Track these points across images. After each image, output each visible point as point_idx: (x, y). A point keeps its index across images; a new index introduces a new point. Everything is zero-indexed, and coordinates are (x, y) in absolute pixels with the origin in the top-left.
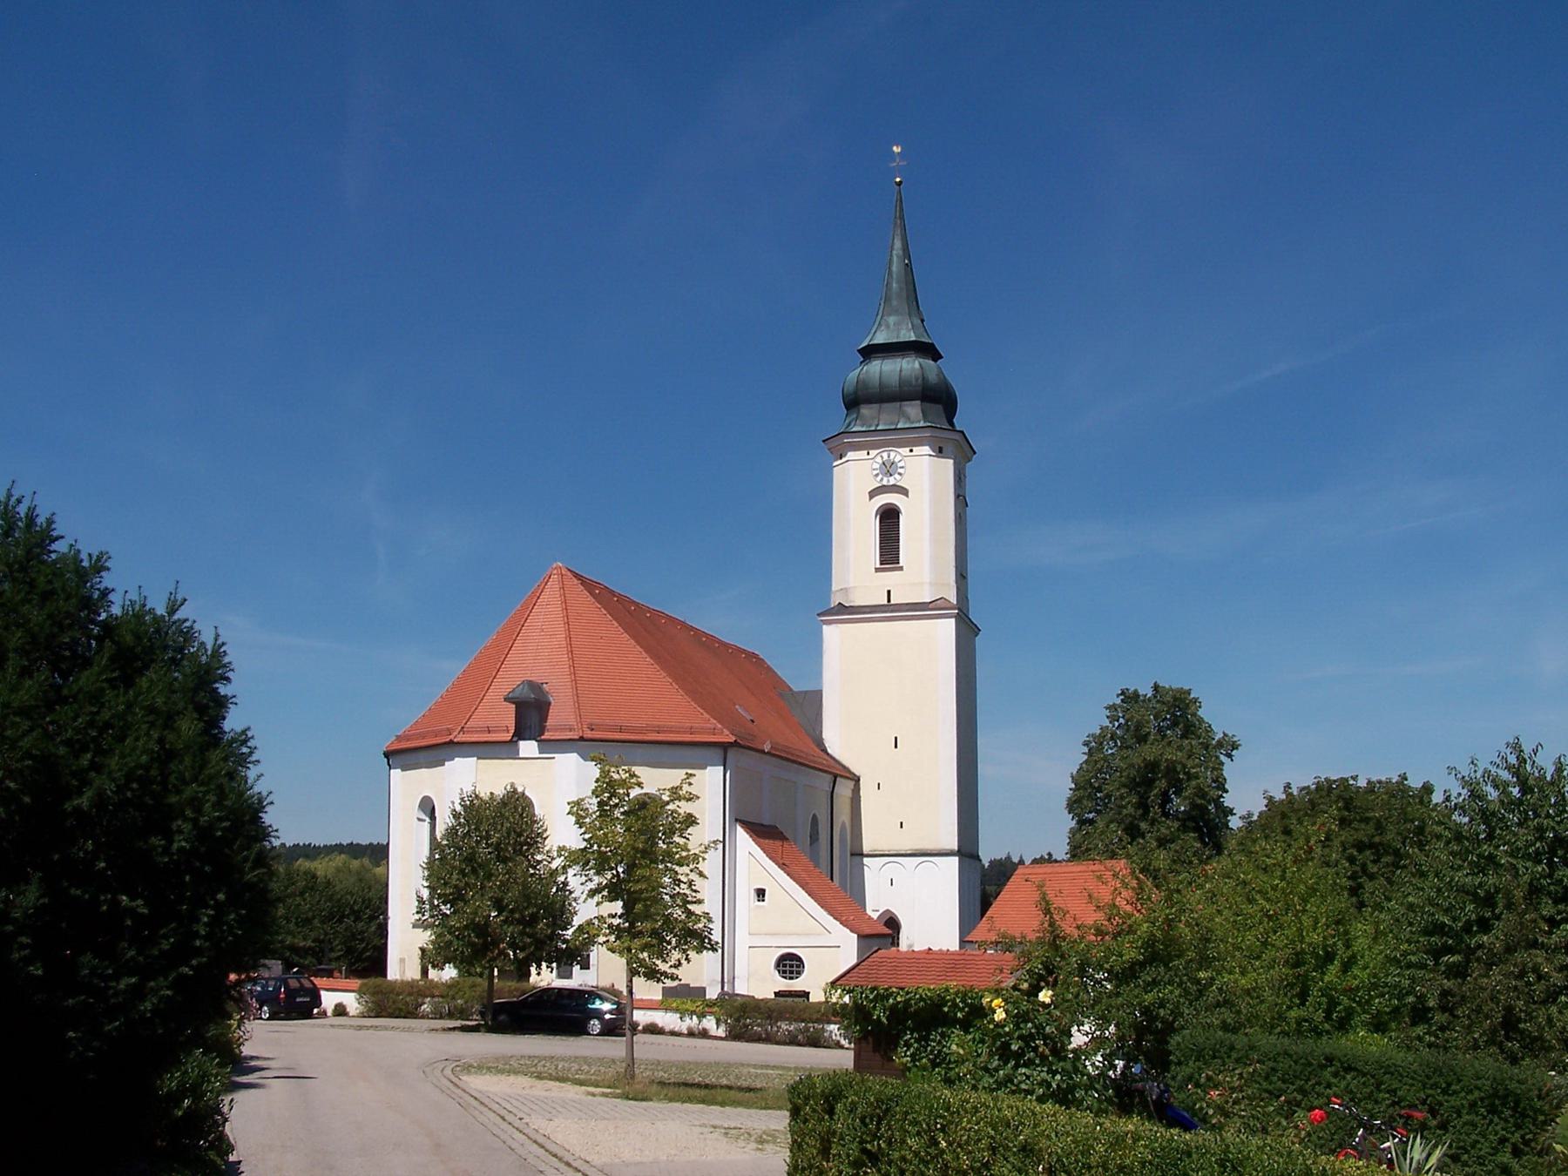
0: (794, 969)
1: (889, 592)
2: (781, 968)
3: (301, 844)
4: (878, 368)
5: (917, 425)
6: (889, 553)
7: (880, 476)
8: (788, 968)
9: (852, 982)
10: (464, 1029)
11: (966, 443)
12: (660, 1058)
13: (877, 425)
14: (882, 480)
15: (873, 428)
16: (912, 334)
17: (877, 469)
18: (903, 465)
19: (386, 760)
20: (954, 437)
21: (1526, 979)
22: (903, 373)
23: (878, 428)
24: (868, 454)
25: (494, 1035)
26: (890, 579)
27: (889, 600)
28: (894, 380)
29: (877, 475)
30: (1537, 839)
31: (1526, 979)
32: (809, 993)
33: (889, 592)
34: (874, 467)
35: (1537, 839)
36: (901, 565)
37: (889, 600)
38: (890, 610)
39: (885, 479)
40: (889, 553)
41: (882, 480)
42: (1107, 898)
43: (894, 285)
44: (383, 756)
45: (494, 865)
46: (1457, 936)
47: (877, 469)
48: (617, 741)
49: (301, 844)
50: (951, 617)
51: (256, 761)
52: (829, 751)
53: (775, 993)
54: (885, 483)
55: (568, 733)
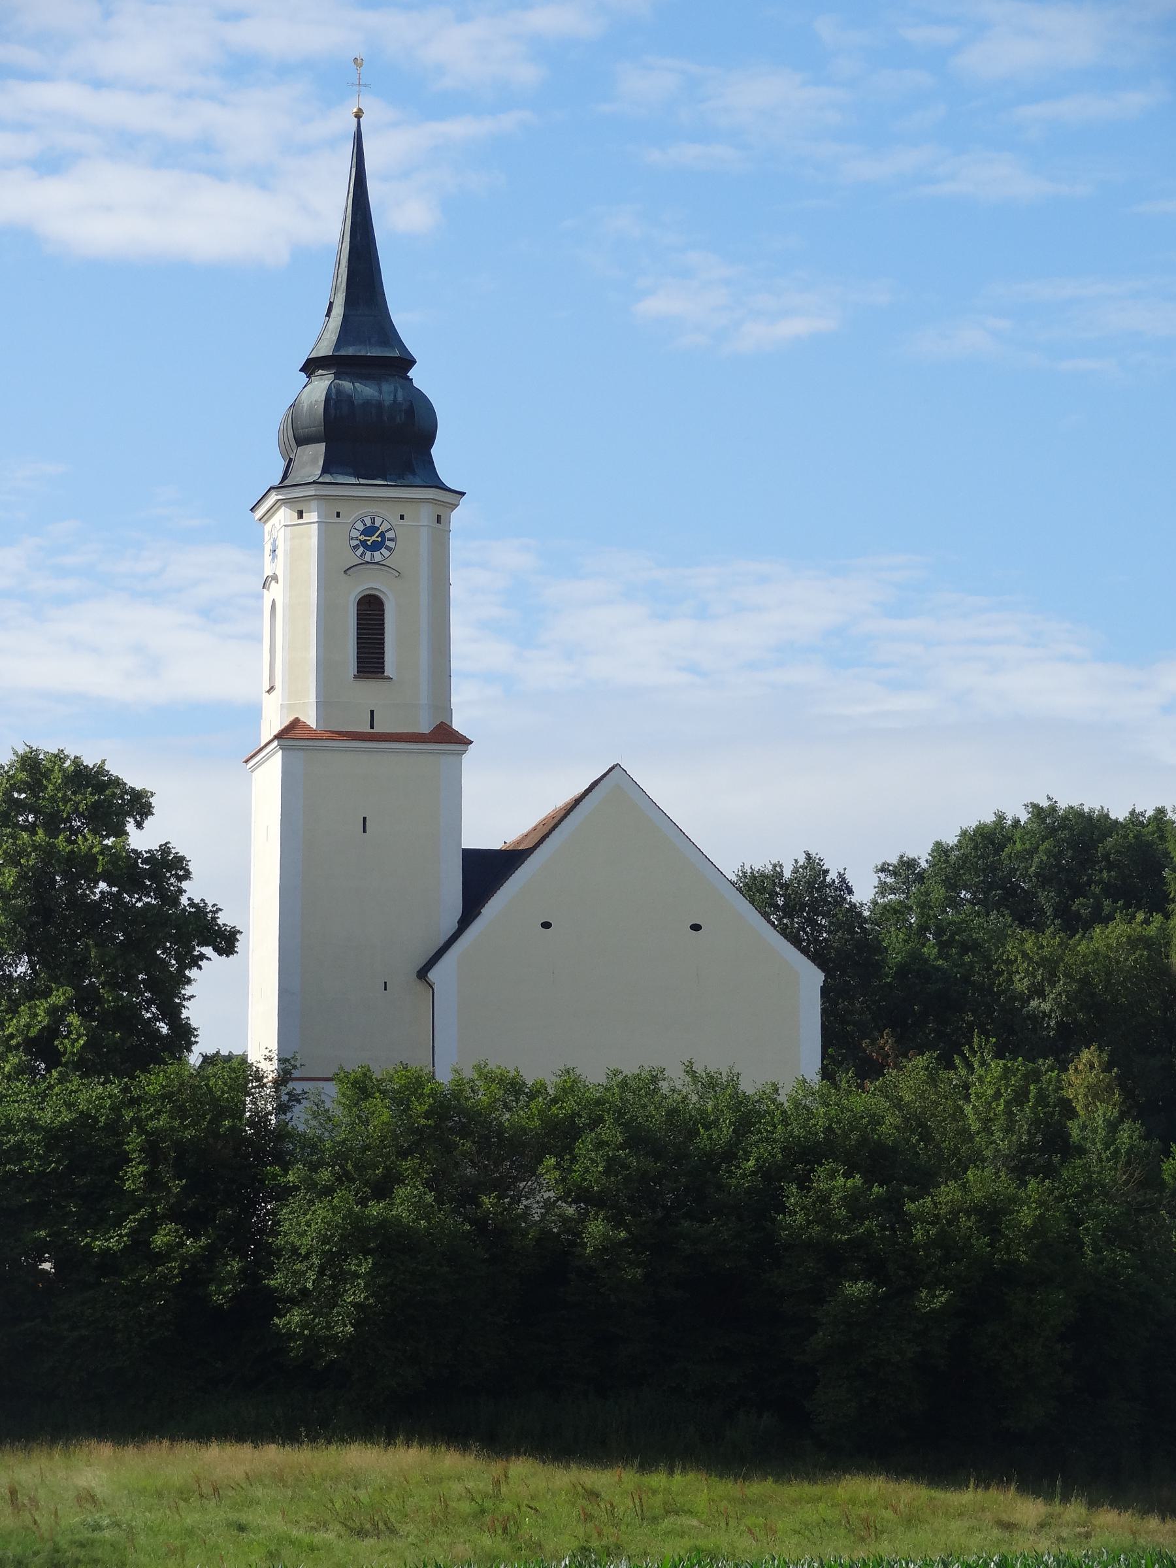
7: (361, 549)
14: (363, 554)
27: (372, 727)
37: (372, 727)
39: (368, 553)
41: (363, 554)
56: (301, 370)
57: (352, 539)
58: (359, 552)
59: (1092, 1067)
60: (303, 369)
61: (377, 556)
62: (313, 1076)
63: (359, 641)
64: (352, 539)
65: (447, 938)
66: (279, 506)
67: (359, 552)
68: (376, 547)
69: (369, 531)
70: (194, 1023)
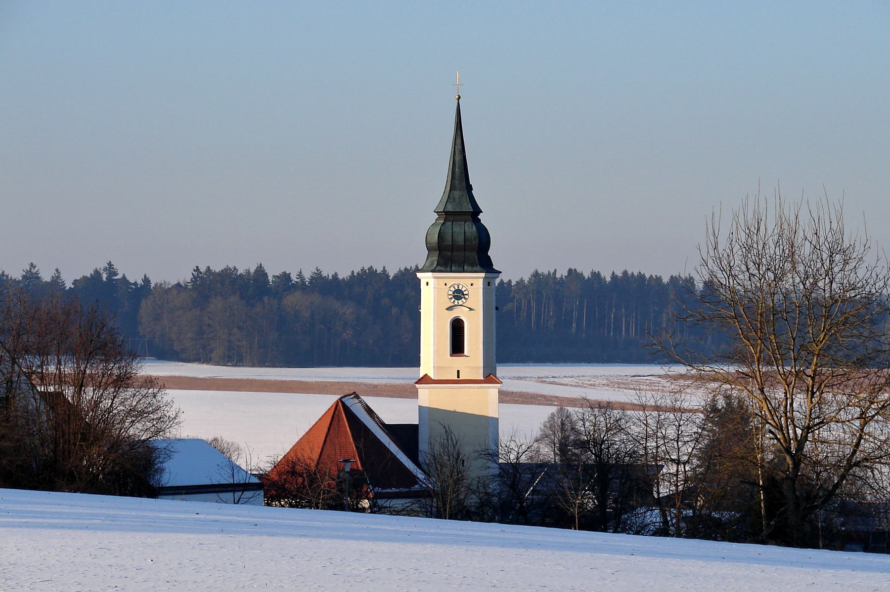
1: (458, 371)
6: (457, 347)
9: (461, 269)
12: (186, 502)
14: (454, 302)
16: (471, 207)
18: (467, 293)
21: (570, 453)
22: (467, 234)
26: (458, 362)
27: (458, 377)
29: (451, 298)
30: (737, 436)
31: (570, 453)
33: (458, 371)
34: (449, 293)
35: (737, 436)
37: (458, 377)
39: (456, 301)
40: (457, 347)
41: (454, 302)
42: (683, 430)
43: (457, 169)
51: (476, 452)
54: (456, 303)
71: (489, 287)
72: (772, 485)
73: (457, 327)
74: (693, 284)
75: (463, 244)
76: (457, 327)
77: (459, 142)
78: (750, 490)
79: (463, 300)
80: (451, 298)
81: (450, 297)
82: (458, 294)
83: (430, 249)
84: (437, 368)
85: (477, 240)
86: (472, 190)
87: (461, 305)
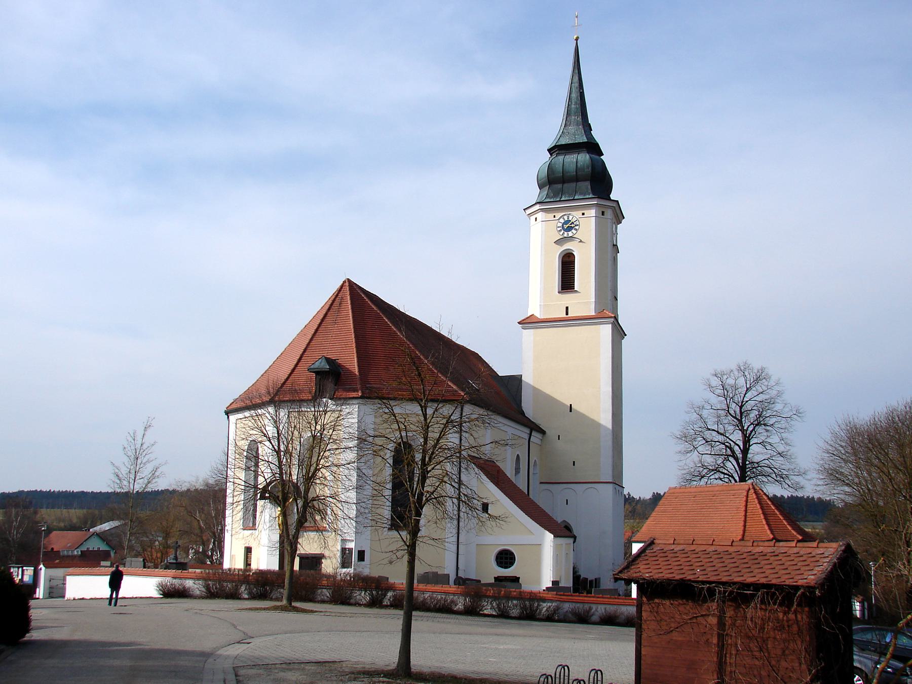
0: (508, 556)
1: (567, 308)
2: (499, 560)
3: (61, 491)
4: (561, 160)
5: (588, 197)
6: (567, 283)
7: (563, 231)
8: (504, 560)
10: (275, 608)
11: (619, 210)
13: (561, 198)
14: (564, 233)
15: (558, 200)
16: (585, 138)
17: (560, 227)
19: (226, 416)
20: (612, 205)
23: (562, 199)
24: (554, 216)
25: (555, 397)
26: (568, 299)
27: (567, 314)
28: (571, 168)
29: (561, 230)
32: (519, 578)
33: (567, 308)
34: (558, 226)
36: (575, 289)
37: (567, 314)
38: (568, 320)
39: (566, 233)
40: (567, 283)
41: (564, 233)
44: (224, 413)
45: (437, 450)
46: (716, 470)
47: (560, 227)
48: (521, 431)
49: (61, 491)
50: (608, 323)
52: (526, 415)
53: (495, 578)
54: (565, 235)
55: (353, 393)
56: (519, 578)
57: (558, 227)
58: (561, 233)
59: (302, 628)
60: (549, 150)
61: (570, 234)
62: (530, 451)
63: (563, 266)
64: (558, 227)
65: (572, 624)
66: (525, 432)
67: (561, 233)
68: (569, 229)
69: (566, 222)
70: (58, 490)
71: (603, 216)
72: (870, 440)
73: (567, 264)
74: (591, 610)
75: (575, 173)
76: (567, 264)
77: (576, 79)
78: (455, 417)
79: (573, 231)
80: (561, 230)
81: (559, 229)
82: (569, 226)
83: (541, 187)
84: (544, 307)
85: (590, 168)
86: (592, 130)
87: (571, 237)
